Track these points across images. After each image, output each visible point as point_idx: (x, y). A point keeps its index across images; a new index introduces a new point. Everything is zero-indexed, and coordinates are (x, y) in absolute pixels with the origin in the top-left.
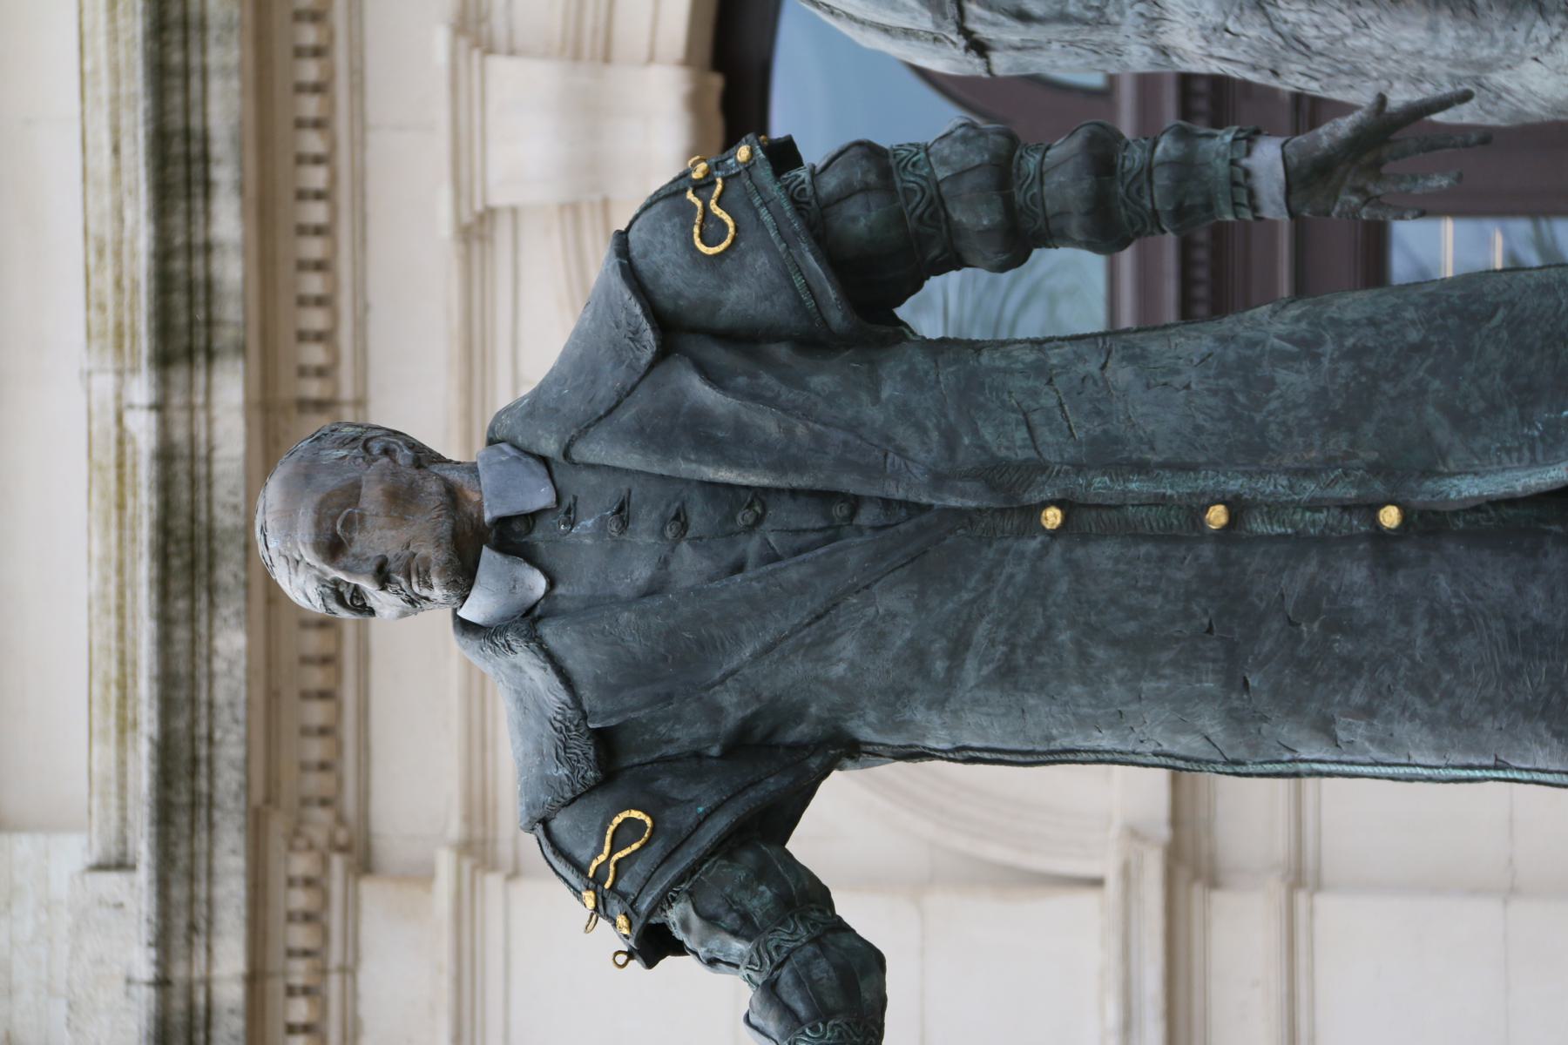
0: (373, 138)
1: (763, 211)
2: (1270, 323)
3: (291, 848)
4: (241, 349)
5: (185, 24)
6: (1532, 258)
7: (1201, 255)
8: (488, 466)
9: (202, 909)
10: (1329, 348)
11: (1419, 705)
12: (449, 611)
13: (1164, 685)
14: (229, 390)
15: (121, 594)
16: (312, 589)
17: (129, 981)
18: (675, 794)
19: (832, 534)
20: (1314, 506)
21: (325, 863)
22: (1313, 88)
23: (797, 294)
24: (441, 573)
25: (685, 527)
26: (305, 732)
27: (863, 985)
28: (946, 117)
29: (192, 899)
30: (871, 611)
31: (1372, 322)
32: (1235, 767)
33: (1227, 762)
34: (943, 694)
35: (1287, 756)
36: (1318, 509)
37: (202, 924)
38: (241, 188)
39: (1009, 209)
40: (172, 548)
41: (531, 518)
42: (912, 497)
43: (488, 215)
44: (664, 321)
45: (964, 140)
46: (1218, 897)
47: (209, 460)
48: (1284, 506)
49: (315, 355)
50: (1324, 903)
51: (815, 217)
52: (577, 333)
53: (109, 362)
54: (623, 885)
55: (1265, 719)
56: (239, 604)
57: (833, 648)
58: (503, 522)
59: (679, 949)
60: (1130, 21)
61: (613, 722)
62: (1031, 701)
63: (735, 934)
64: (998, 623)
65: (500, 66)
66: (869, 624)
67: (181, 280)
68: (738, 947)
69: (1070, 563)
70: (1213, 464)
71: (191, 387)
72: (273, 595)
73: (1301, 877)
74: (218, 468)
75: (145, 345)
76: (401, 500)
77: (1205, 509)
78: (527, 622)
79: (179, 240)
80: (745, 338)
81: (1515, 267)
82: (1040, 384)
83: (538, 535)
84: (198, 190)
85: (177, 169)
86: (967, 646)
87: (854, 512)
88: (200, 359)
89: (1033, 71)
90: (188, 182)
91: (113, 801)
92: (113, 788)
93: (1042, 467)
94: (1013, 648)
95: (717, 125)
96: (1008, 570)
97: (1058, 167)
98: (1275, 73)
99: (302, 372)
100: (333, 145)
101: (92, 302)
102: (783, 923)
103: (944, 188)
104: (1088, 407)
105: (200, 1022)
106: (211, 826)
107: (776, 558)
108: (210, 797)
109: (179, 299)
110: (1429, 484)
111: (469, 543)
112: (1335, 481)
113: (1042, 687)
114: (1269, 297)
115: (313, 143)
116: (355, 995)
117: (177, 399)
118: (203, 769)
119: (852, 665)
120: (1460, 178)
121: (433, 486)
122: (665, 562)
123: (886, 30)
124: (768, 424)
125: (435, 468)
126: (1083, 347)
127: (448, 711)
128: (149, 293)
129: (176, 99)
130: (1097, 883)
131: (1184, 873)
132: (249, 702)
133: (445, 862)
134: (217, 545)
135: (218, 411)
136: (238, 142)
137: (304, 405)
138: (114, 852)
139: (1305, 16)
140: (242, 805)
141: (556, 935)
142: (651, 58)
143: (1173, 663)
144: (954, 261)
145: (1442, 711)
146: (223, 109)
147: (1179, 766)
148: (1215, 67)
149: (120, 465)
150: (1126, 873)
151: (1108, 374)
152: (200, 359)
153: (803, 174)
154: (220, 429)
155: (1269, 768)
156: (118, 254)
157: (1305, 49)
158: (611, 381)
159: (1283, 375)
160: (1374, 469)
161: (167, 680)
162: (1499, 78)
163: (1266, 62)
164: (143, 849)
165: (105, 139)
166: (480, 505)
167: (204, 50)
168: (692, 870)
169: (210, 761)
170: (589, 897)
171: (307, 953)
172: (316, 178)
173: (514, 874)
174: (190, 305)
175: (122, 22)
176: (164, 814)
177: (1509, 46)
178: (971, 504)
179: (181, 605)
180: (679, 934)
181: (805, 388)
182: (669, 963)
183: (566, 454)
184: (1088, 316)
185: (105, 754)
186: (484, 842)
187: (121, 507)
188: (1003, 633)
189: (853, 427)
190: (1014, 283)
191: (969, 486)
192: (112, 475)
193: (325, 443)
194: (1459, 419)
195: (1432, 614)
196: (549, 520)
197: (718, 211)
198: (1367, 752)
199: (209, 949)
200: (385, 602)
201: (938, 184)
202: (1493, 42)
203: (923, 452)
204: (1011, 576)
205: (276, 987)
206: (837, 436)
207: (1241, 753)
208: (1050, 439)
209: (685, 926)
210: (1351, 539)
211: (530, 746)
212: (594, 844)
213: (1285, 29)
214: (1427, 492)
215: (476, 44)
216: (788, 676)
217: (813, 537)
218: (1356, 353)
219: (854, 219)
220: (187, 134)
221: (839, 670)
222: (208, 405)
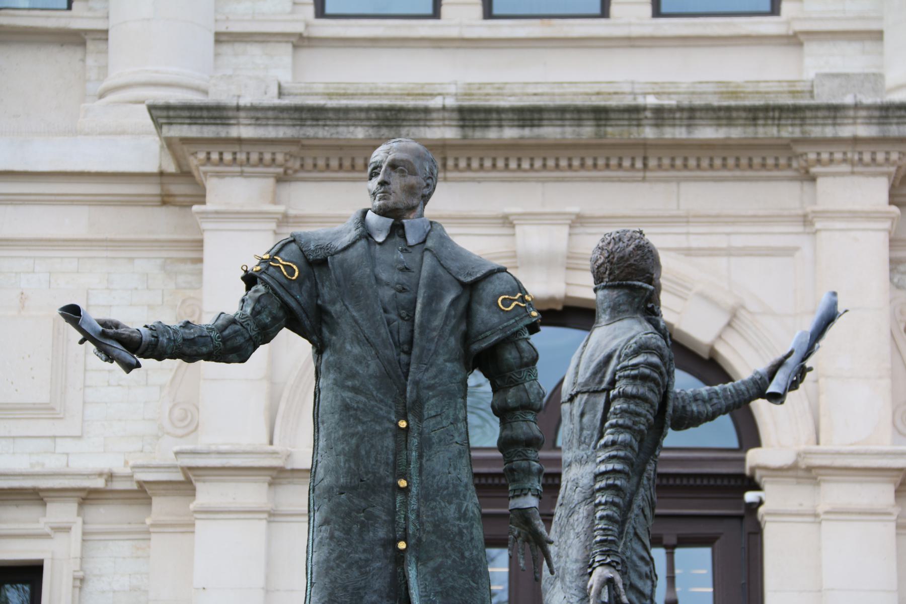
0: (539, 185)
1: (513, 321)
2: (472, 503)
3: (286, 154)
4: (465, 137)
5: (580, 119)
7: (497, 481)
8: (423, 222)
9: (264, 122)
10: (463, 524)
11: (334, 555)
12: (370, 207)
13: (342, 464)
14: (450, 133)
15: (377, 94)
16: (378, 158)
17: (239, 97)
18: (304, 287)
19: (398, 345)
20: (406, 518)
21: (280, 166)
22: (556, 519)
23: (484, 332)
24: (384, 204)
25: (400, 292)
26: (328, 159)
27: (234, 355)
28: (548, 389)
29: (268, 119)
30: (369, 358)
31: (472, 539)
32: (312, 490)
33: (314, 487)
34: (339, 384)
35: (316, 508)
36: (405, 520)
37: (259, 122)
38: (522, 138)
39: (515, 409)
40: (393, 113)
41: (404, 237)
42: (410, 374)
43: (512, 225)
44: (475, 285)
45: (539, 393)
46: (266, 485)
47: (425, 126)
48: (406, 508)
49: (463, 164)
51: (511, 339)
52: (470, 254)
53: (460, 91)
54: (271, 269)
55: (329, 500)
56: (373, 136)
57: (356, 345)
59: (248, 289)
60: (580, 453)
61: (330, 266)
62: (336, 416)
63: (253, 309)
64: (365, 404)
65: (565, 230)
66: (365, 358)
67: (489, 117)
68: (248, 310)
69: (386, 431)
70: (421, 482)
71: (450, 119)
72: (375, 147)
73: (272, 515)
74: (422, 129)
75: (466, 104)
76: (411, 190)
77: (405, 479)
78: (366, 235)
79: (503, 116)
80: (468, 314)
81: (492, 595)
82: (451, 420)
83: (398, 239)
84: (521, 123)
85: (529, 116)
86: (356, 393)
87: (405, 353)
88: (461, 123)
89: (563, 418)
90: (524, 120)
91: (303, 91)
92: (308, 91)
93: (421, 420)
94: (356, 410)
95: (545, 307)
96: (384, 408)
97: (529, 427)
98: (561, 505)
99: (456, 159)
100: (537, 171)
101: (481, 86)
102: (257, 326)
103: (521, 386)
104: (442, 437)
105: (224, 121)
106: (294, 125)
107: (389, 324)
108: (304, 125)
110: (414, 559)
111: (395, 215)
112: (415, 526)
113: (341, 420)
114: (481, 505)
115: (538, 164)
116: (234, 176)
117: (447, 115)
118: (315, 123)
119: (350, 352)
120: (523, 570)
121: (415, 202)
122: (388, 285)
123: (578, 366)
124: (437, 322)
125: (422, 202)
126: (464, 436)
127: (334, 209)
129: (553, 116)
131: (274, 473)
132: (338, 139)
133: (280, 208)
134: (395, 128)
135: (442, 129)
136: (538, 137)
137: (445, 160)
138: (285, 91)
139: (581, 515)
140: (301, 136)
141: (252, 246)
142: (568, 284)
143: (350, 467)
144: (495, 390)
145: (332, 564)
146: (550, 132)
147: (313, 471)
148: (563, 484)
149: (423, 95)
151: (455, 444)
152: (461, 123)
153: (527, 335)
154: (436, 130)
155: (312, 502)
156: (498, 94)
158: (453, 266)
160: (419, 540)
162: (558, 584)
163: (565, 501)
165: (540, 90)
166: (409, 218)
167: (571, 126)
168: (276, 293)
169: (318, 125)
170: (267, 256)
171: (248, 159)
172: (526, 165)
173: (275, 233)
174: (480, 120)
175: (580, 97)
176: (298, 109)
177: (570, 588)
178: (408, 395)
179: (373, 115)
180: (253, 289)
181: (450, 335)
182: (243, 285)
183: (427, 249)
184: (476, 441)
185: (320, 88)
186: (287, 222)
187: (408, 95)
188: (361, 406)
189: (436, 352)
190: (489, 414)
191: (414, 394)
192: (420, 92)
193: (431, 164)
194: (437, 570)
195: (367, 560)
196: (403, 243)
197: (514, 304)
198: (317, 536)
199: (250, 125)
200: (374, 184)
201: (523, 384)
202: (571, 582)
203: (427, 378)
204: (381, 409)
205: (236, 148)
206: (433, 347)
207: (317, 492)
208: (431, 423)
209: (256, 291)
210: (394, 531)
211: (321, 236)
212: (286, 258)
213: (577, 508)
214: (411, 559)
215: (573, 222)
216: (346, 328)
217: (396, 337)
218: (461, 533)
219: (510, 353)
220: (541, 119)
221: (348, 347)
222: (445, 126)
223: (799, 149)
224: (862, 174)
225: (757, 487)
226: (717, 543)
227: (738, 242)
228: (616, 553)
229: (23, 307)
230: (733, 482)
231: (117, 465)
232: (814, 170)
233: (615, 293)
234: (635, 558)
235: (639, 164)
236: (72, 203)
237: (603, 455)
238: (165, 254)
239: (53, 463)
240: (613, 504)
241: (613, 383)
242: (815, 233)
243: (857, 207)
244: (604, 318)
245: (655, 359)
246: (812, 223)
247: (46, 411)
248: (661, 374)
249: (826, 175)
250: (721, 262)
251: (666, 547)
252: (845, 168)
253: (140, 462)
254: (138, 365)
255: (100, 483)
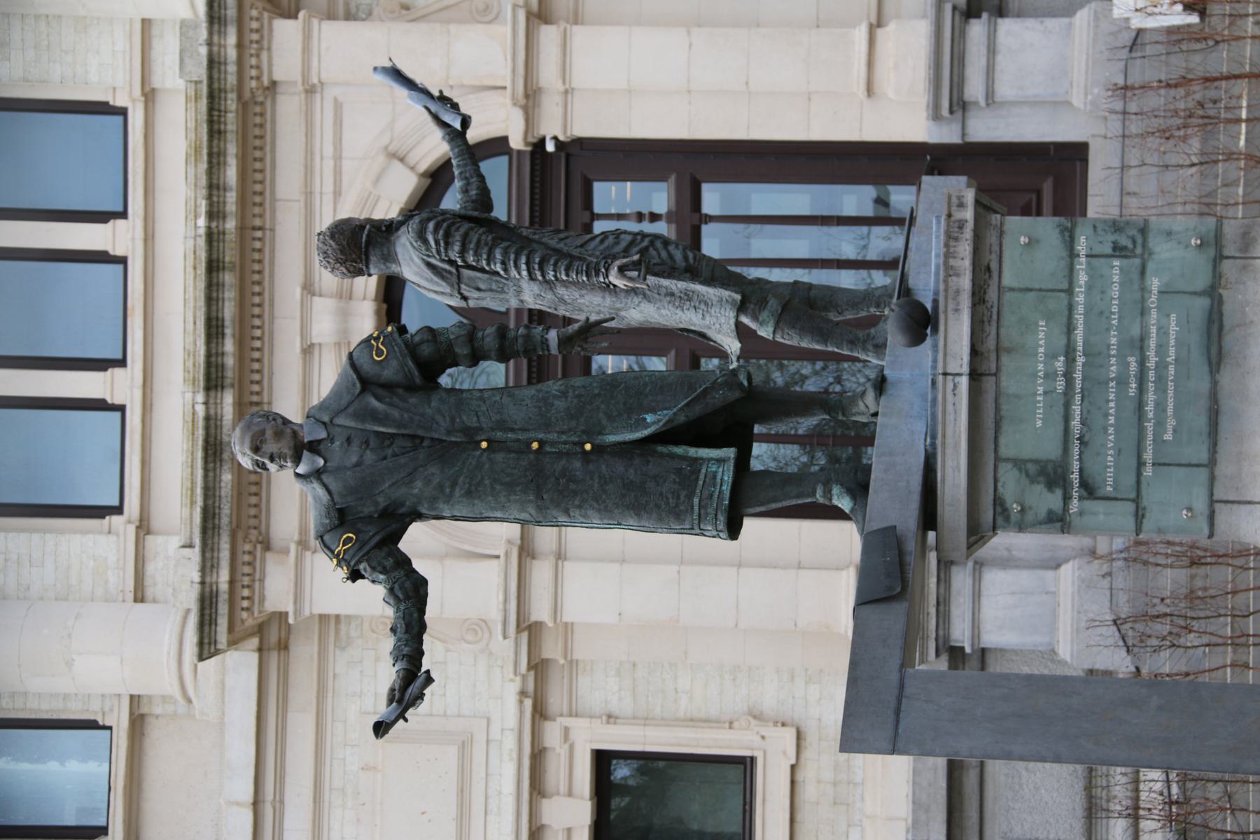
0: (276, 321)
2: (553, 386)
4: (232, 386)
6: (636, 368)
14: (228, 399)
16: (249, 462)
19: (415, 448)
20: (565, 443)
22: (567, 314)
26: (250, 506)
29: (212, 557)
31: (584, 387)
32: (539, 523)
34: (449, 499)
38: (234, 336)
39: (473, 348)
41: (320, 441)
44: (363, 379)
46: (534, 562)
49: (256, 388)
50: (566, 563)
51: (412, 349)
58: (310, 442)
59: (363, 577)
65: (316, 299)
68: (382, 577)
69: (490, 459)
70: (534, 429)
73: (560, 556)
74: (224, 423)
75: (202, 384)
76: (278, 435)
78: (317, 474)
80: (389, 387)
85: (214, 329)
93: (481, 429)
95: (385, 319)
97: (488, 335)
99: (252, 393)
101: (186, 370)
109: (213, 370)
111: (299, 449)
114: (555, 378)
115: (257, 322)
117: (212, 401)
121: (288, 431)
123: (436, 292)
124: (396, 413)
127: (293, 501)
128: (280, 310)
129: (214, 308)
130: (498, 557)
131: (524, 554)
133: (293, 547)
136: (233, 321)
137: (252, 404)
144: (456, 364)
146: (229, 311)
147: (523, 523)
148: (538, 307)
150: (507, 554)
157: (565, 303)
158: (346, 399)
159: (557, 403)
160: (584, 432)
161: (206, 489)
162: (623, 313)
164: (197, 541)
165: (191, 319)
168: (368, 553)
170: (335, 561)
172: (258, 333)
173: (315, 552)
179: (211, 465)
182: (360, 581)
184: (499, 381)
185: (186, 512)
189: (422, 415)
194: (610, 417)
200: (272, 467)
203: (444, 424)
205: (239, 585)
206: (417, 418)
210: (576, 454)
216: (401, 492)
218: (579, 396)
221: (416, 491)
223: (247, 95)
224: (270, 42)
225: (542, 141)
226: (590, 176)
227: (329, 150)
228: (597, 264)
229: (375, 768)
230: (538, 162)
231: (513, 688)
232: (266, 82)
233: (373, 258)
234: (602, 247)
235: (259, 234)
236: (284, 727)
237: (514, 273)
238: (331, 647)
239: (510, 742)
240: (555, 265)
241: (451, 262)
242: (322, 83)
243: (299, 47)
244: (394, 268)
245: (431, 225)
246: (314, 86)
247: (465, 748)
248: (444, 221)
249: (270, 72)
250: (347, 165)
251: (592, 220)
252: (264, 55)
253: (511, 669)
254: (428, 672)
255: (528, 703)
